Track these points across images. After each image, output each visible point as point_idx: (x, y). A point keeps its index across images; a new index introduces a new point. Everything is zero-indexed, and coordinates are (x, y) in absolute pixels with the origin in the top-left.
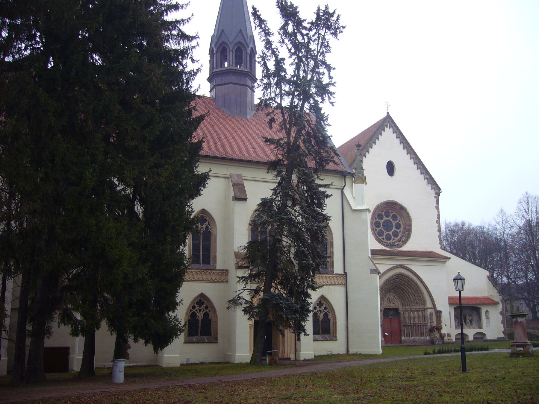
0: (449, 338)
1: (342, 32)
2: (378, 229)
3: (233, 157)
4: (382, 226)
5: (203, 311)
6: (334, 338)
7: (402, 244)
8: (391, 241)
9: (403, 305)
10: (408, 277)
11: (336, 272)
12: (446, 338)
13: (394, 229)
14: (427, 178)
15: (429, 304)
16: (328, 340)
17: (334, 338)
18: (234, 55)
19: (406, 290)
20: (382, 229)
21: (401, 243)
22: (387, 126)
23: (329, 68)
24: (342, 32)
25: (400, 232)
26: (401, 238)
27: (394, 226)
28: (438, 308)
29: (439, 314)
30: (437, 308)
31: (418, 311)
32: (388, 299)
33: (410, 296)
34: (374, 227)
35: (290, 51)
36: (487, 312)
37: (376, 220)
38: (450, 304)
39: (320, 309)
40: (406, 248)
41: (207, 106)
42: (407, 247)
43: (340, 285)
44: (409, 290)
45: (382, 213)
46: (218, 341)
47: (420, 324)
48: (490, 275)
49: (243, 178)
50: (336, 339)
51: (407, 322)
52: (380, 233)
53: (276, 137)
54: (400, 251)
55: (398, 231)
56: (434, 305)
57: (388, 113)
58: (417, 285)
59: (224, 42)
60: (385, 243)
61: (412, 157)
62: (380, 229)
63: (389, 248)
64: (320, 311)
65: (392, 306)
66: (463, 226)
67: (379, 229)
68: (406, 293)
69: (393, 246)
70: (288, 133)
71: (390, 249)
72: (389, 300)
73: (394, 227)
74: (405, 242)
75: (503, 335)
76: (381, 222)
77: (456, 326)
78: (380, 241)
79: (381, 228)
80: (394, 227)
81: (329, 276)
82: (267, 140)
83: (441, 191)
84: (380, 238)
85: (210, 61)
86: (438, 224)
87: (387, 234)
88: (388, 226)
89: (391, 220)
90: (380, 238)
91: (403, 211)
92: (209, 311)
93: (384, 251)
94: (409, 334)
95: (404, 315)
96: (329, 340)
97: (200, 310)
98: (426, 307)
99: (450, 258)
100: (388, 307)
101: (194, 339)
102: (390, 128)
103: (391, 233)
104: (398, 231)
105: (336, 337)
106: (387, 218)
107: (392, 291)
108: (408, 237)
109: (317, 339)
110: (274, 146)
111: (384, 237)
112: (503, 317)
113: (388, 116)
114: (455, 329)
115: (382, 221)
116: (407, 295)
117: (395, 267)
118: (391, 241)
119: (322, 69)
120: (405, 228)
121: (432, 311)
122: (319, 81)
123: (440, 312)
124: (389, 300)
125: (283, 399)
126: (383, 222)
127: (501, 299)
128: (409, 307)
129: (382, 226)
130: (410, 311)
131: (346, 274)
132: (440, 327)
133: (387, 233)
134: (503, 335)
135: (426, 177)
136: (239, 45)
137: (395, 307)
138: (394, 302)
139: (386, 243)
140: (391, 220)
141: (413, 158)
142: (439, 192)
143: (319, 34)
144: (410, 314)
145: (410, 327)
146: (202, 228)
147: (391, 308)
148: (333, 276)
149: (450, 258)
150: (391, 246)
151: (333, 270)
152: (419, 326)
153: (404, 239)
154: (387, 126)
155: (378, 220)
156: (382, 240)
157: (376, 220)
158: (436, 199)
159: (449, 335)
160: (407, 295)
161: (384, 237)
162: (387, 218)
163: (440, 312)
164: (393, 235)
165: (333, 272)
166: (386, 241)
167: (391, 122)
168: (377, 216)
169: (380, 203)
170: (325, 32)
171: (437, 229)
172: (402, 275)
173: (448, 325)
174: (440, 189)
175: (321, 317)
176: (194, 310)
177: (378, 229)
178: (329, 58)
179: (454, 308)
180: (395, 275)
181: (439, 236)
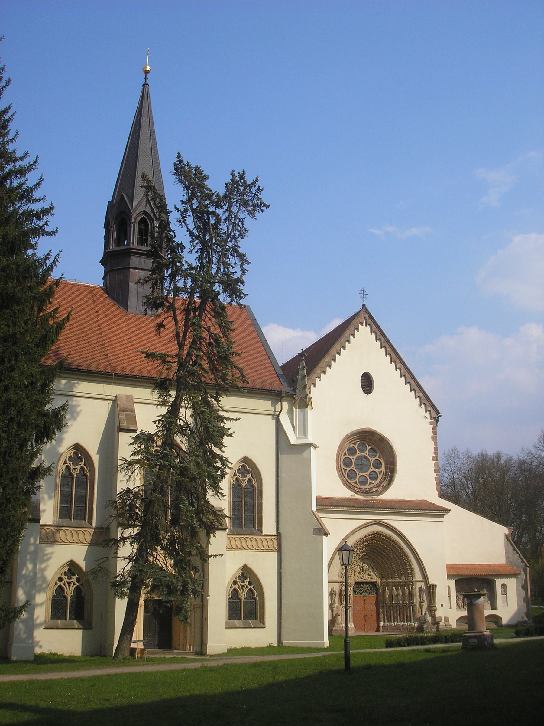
0: (446, 623)
1: (262, 211)
2: (348, 469)
3: (121, 372)
4: (353, 465)
5: (247, 587)
6: (261, 624)
7: (382, 491)
8: (367, 486)
9: (382, 577)
12: (442, 624)
13: (372, 469)
14: (419, 397)
15: (418, 576)
16: (251, 628)
17: (261, 624)
18: (136, 229)
19: (386, 555)
20: (354, 469)
21: (380, 489)
22: (362, 324)
23: (242, 257)
24: (262, 211)
25: (380, 472)
26: (381, 482)
27: (372, 465)
28: (431, 581)
29: (431, 590)
30: (430, 581)
31: (403, 587)
32: (361, 568)
33: (392, 564)
34: (343, 466)
35: (191, 234)
36: (504, 586)
37: (346, 456)
38: (450, 576)
39: (243, 584)
40: (390, 495)
41: (95, 299)
42: (390, 495)
43: (269, 550)
44: (391, 556)
46: (93, 626)
47: (405, 603)
48: (509, 533)
49: (134, 400)
50: (264, 626)
51: (388, 602)
52: (352, 475)
53: (159, 350)
54: (380, 501)
55: (377, 471)
57: (364, 305)
58: (402, 549)
59: (122, 211)
60: (357, 489)
61: (398, 367)
62: (351, 468)
63: (364, 496)
64: (242, 586)
65: (367, 579)
66: (499, 461)
67: (350, 469)
68: (385, 560)
69: (369, 493)
70: (181, 345)
71: (364, 498)
72: (363, 570)
73: (372, 466)
74: (386, 488)
75: (526, 619)
76: (353, 458)
78: (349, 487)
79: (353, 467)
80: (372, 466)
81: (271, 538)
82: (148, 356)
83: (439, 415)
84: (351, 482)
85: (105, 237)
86: (435, 462)
88: (362, 464)
90: (351, 482)
92: (64, 584)
94: (391, 619)
95: (384, 591)
96: (254, 628)
97: (69, 583)
98: (414, 580)
99: (450, 510)
100: (360, 580)
101: (236, 622)
102: (366, 327)
103: (367, 474)
104: (377, 471)
105: (264, 624)
106: (361, 454)
107: (367, 557)
108: (391, 481)
109: (237, 626)
110: (157, 363)
111: (357, 480)
112: (525, 592)
114: (457, 611)
115: (355, 457)
116: (388, 562)
117: (369, 523)
118: (367, 486)
119: (232, 260)
120: (386, 468)
121: (423, 585)
122: (227, 274)
123: (434, 586)
124: (363, 570)
127: (523, 567)
128: (391, 581)
129: (353, 465)
130: (392, 585)
131: (279, 535)
132: (434, 608)
134: (526, 619)
135: (418, 394)
136: (144, 216)
137: (372, 581)
138: (370, 573)
139: (359, 488)
141: (399, 368)
142: (436, 416)
143: (231, 212)
144: (392, 589)
145: (392, 607)
146: (75, 469)
147: (365, 581)
148: (261, 537)
149: (450, 510)
150: (367, 493)
151: (262, 529)
152: (405, 607)
153: (385, 483)
154: (362, 324)
155: (348, 456)
156: (353, 484)
157: (346, 456)
158: (432, 426)
159: (447, 619)
160: (388, 562)
161: (357, 480)
162: (361, 454)
163: (434, 586)
164: (370, 478)
165: (262, 532)
166: (360, 486)
167: (367, 318)
168: (346, 450)
169: (351, 433)
170: (239, 209)
172: (380, 535)
173: (446, 605)
174: (438, 412)
175: (243, 595)
176: (61, 584)
177: (348, 469)
178: (244, 246)
179: (456, 581)
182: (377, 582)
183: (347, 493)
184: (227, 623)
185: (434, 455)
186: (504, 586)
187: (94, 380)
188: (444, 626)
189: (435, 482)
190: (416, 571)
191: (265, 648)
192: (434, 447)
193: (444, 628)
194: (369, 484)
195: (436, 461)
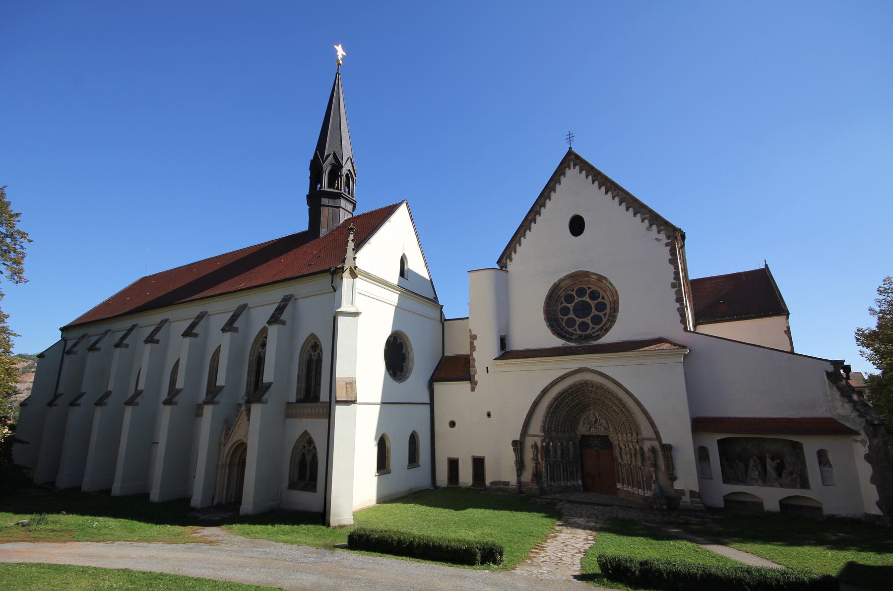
10: (601, 387)
11: (321, 400)
36: (822, 456)
43: (327, 418)
45: (572, 293)
56: (657, 433)
77: (723, 481)
78: (560, 336)
86: (675, 289)
87: (592, 318)
89: (573, 304)
90: (570, 330)
91: (562, 285)
93: (571, 348)
106: (588, 300)
108: (612, 320)
111: (591, 325)
113: (570, 153)
121: (656, 444)
125: (126, 558)
126: (574, 307)
127: (864, 424)
133: (589, 317)
140: (573, 304)
158: (669, 248)
171: (675, 297)
180: (575, 385)
181: (679, 309)
182: (608, 436)
183: (558, 342)
184: (408, 466)
185: (674, 281)
186: (822, 456)
187: (187, 319)
188: (690, 504)
189: (678, 313)
190: (642, 427)
191: (873, 467)
192: (674, 272)
193: (689, 506)
194: (592, 330)
195: (678, 288)
